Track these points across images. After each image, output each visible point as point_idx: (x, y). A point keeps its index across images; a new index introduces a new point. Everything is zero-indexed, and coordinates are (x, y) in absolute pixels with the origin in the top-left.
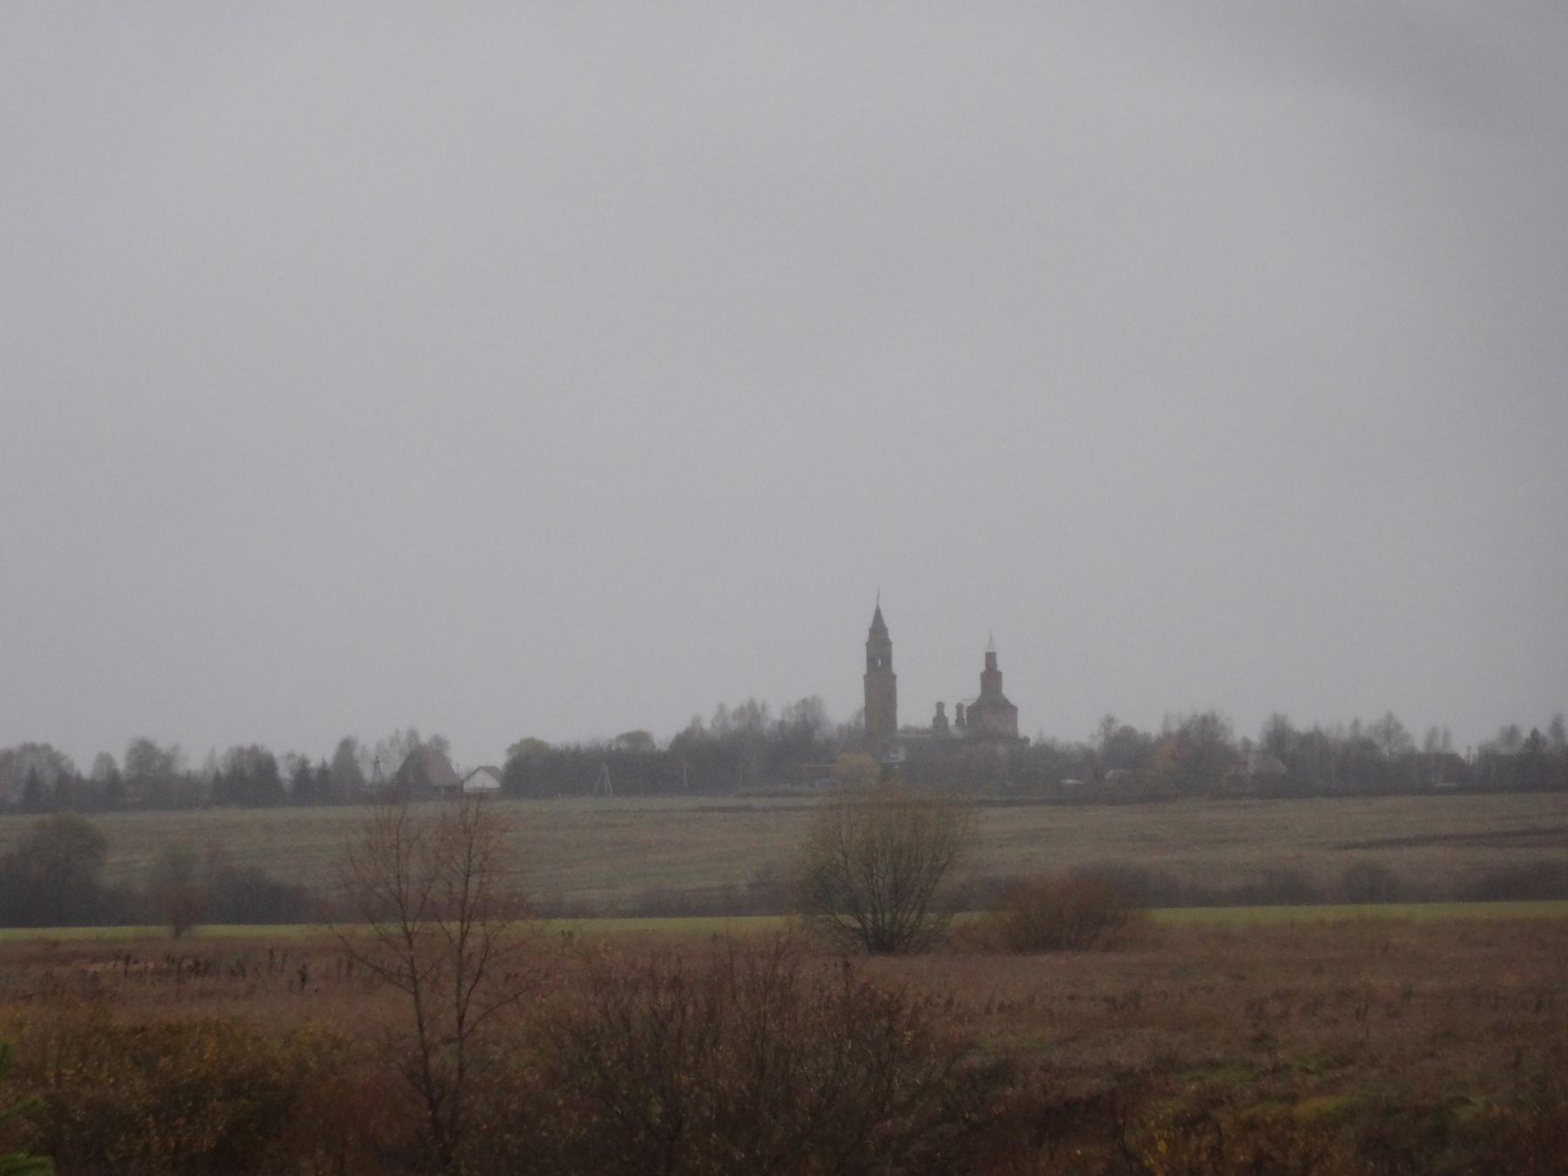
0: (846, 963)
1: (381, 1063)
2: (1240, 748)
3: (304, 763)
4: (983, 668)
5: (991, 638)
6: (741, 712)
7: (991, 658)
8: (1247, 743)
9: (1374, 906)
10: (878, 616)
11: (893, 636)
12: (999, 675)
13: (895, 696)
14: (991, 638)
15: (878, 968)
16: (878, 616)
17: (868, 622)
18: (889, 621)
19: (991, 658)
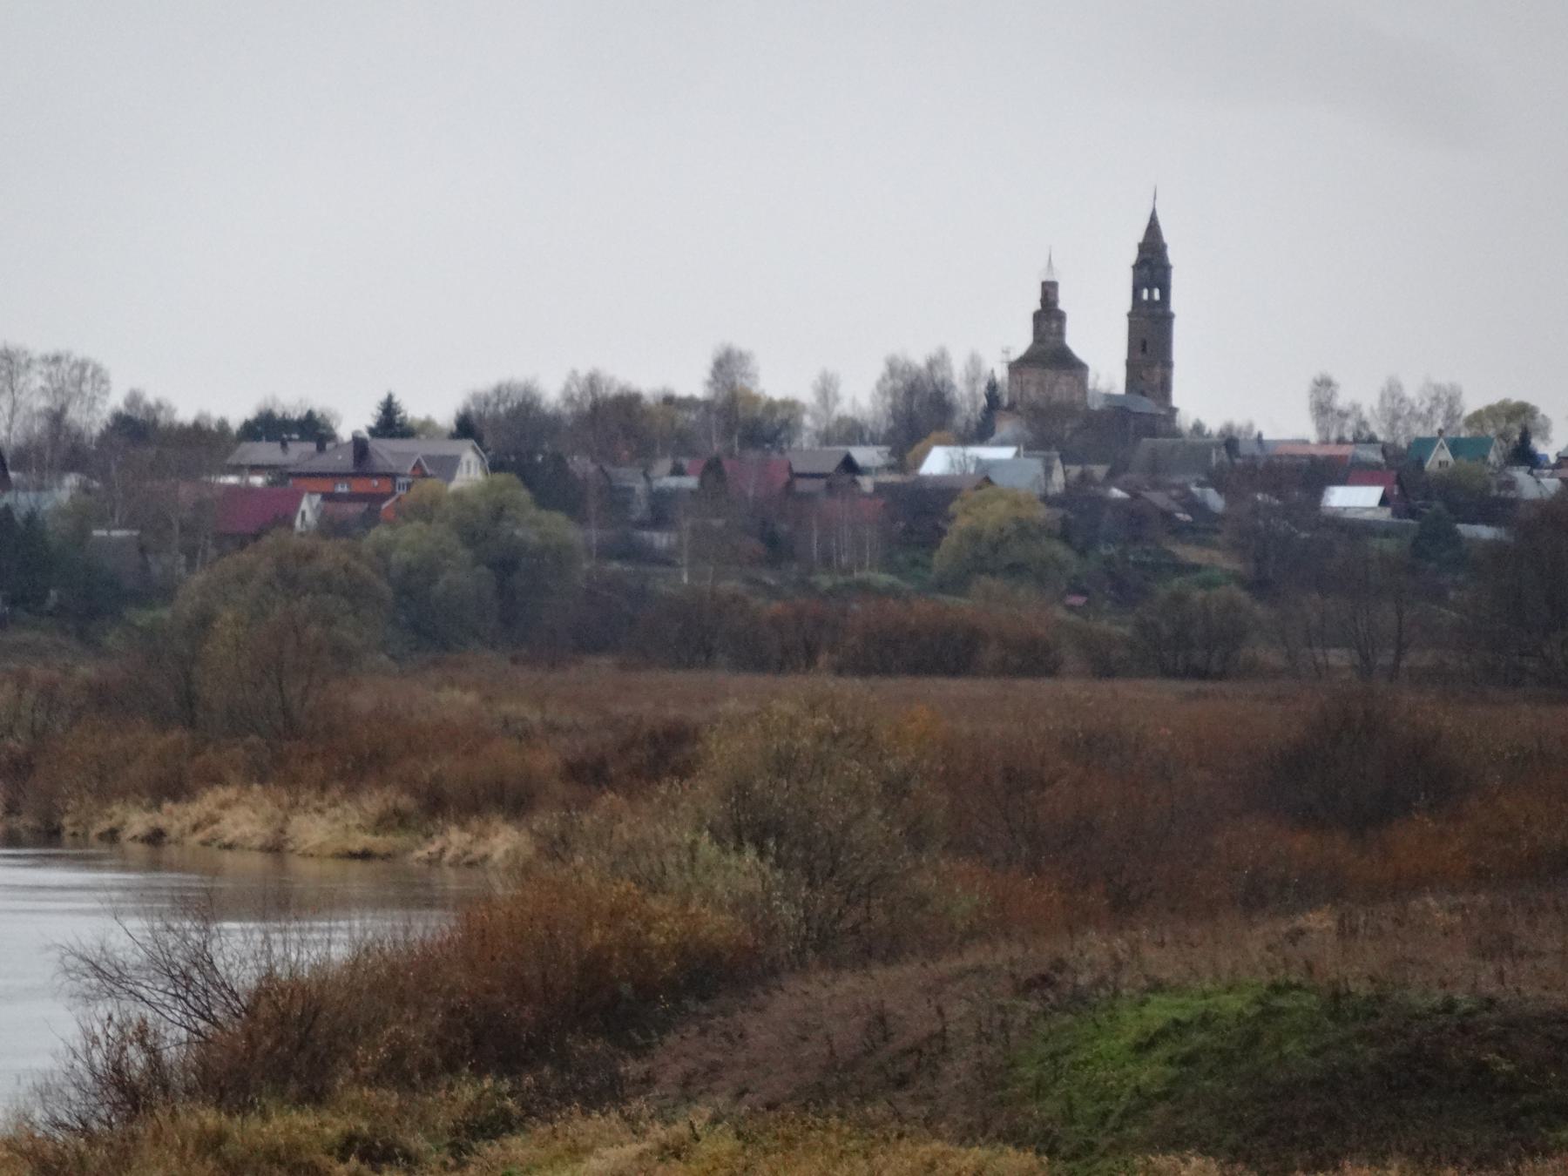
7: (1049, 291)
10: (1153, 229)
11: (1173, 256)
12: (1060, 317)
16: (1153, 229)
19: (1049, 291)
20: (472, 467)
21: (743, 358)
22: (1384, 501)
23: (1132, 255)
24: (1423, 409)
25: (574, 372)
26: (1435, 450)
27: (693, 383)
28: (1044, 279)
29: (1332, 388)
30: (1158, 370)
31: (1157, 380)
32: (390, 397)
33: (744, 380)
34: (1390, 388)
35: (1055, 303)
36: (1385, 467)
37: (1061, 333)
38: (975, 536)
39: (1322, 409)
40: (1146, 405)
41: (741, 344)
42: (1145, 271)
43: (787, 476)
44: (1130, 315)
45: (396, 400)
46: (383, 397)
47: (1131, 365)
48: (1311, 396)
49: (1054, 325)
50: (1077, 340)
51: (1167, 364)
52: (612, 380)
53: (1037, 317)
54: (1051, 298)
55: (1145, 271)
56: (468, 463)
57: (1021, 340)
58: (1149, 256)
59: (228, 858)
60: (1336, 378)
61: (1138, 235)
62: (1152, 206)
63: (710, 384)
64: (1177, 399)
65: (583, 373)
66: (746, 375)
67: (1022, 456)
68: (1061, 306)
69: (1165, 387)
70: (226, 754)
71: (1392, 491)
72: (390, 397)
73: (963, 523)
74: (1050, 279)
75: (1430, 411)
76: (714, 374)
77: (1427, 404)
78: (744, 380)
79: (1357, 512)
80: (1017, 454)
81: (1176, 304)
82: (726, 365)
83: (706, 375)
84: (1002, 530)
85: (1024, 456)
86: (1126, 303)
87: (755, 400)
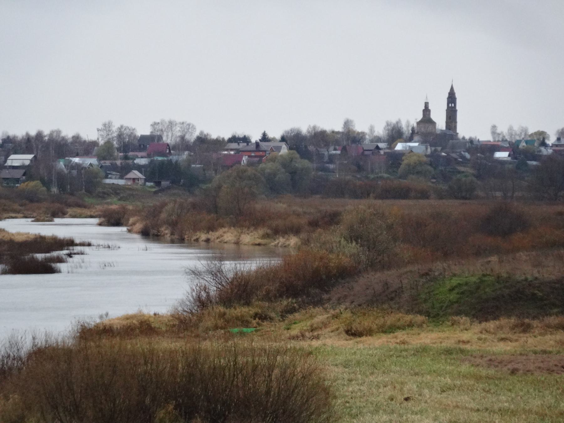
0: (466, 284)
1: (306, 271)
2: (307, 133)
3: (119, 128)
4: (424, 108)
5: (427, 97)
6: (73, 137)
7: (426, 104)
8: (138, 136)
9: (404, 201)
10: (452, 89)
11: (457, 95)
12: (429, 111)
13: (446, 118)
14: (427, 97)
15: (429, 272)
16: (452, 89)
17: (448, 90)
18: (456, 90)
19: (426, 104)
21: (351, 121)
23: (447, 95)
25: (310, 125)
27: (339, 128)
30: (453, 124)
31: (454, 126)
32: (265, 132)
35: (428, 107)
37: (429, 114)
38: (409, 165)
39: (494, 133)
40: (451, 132)
41: (350, 118)
42: (450, 99)
44: (446, 110)
46: (263, 132)
49: (428, 113)
50: (433, 117)
51: (456, 122)
53: (424, 111)
54: (427, 106)
57: (420, 117)
65: (312, 125)
66: (352, 126)
72: (265, 132)
73: (405, 162)
80: (419, 145)
81: (458, 108)
82: (347, 123)
83: (342, 126)
86: (445, 107)
87: (354, 132)
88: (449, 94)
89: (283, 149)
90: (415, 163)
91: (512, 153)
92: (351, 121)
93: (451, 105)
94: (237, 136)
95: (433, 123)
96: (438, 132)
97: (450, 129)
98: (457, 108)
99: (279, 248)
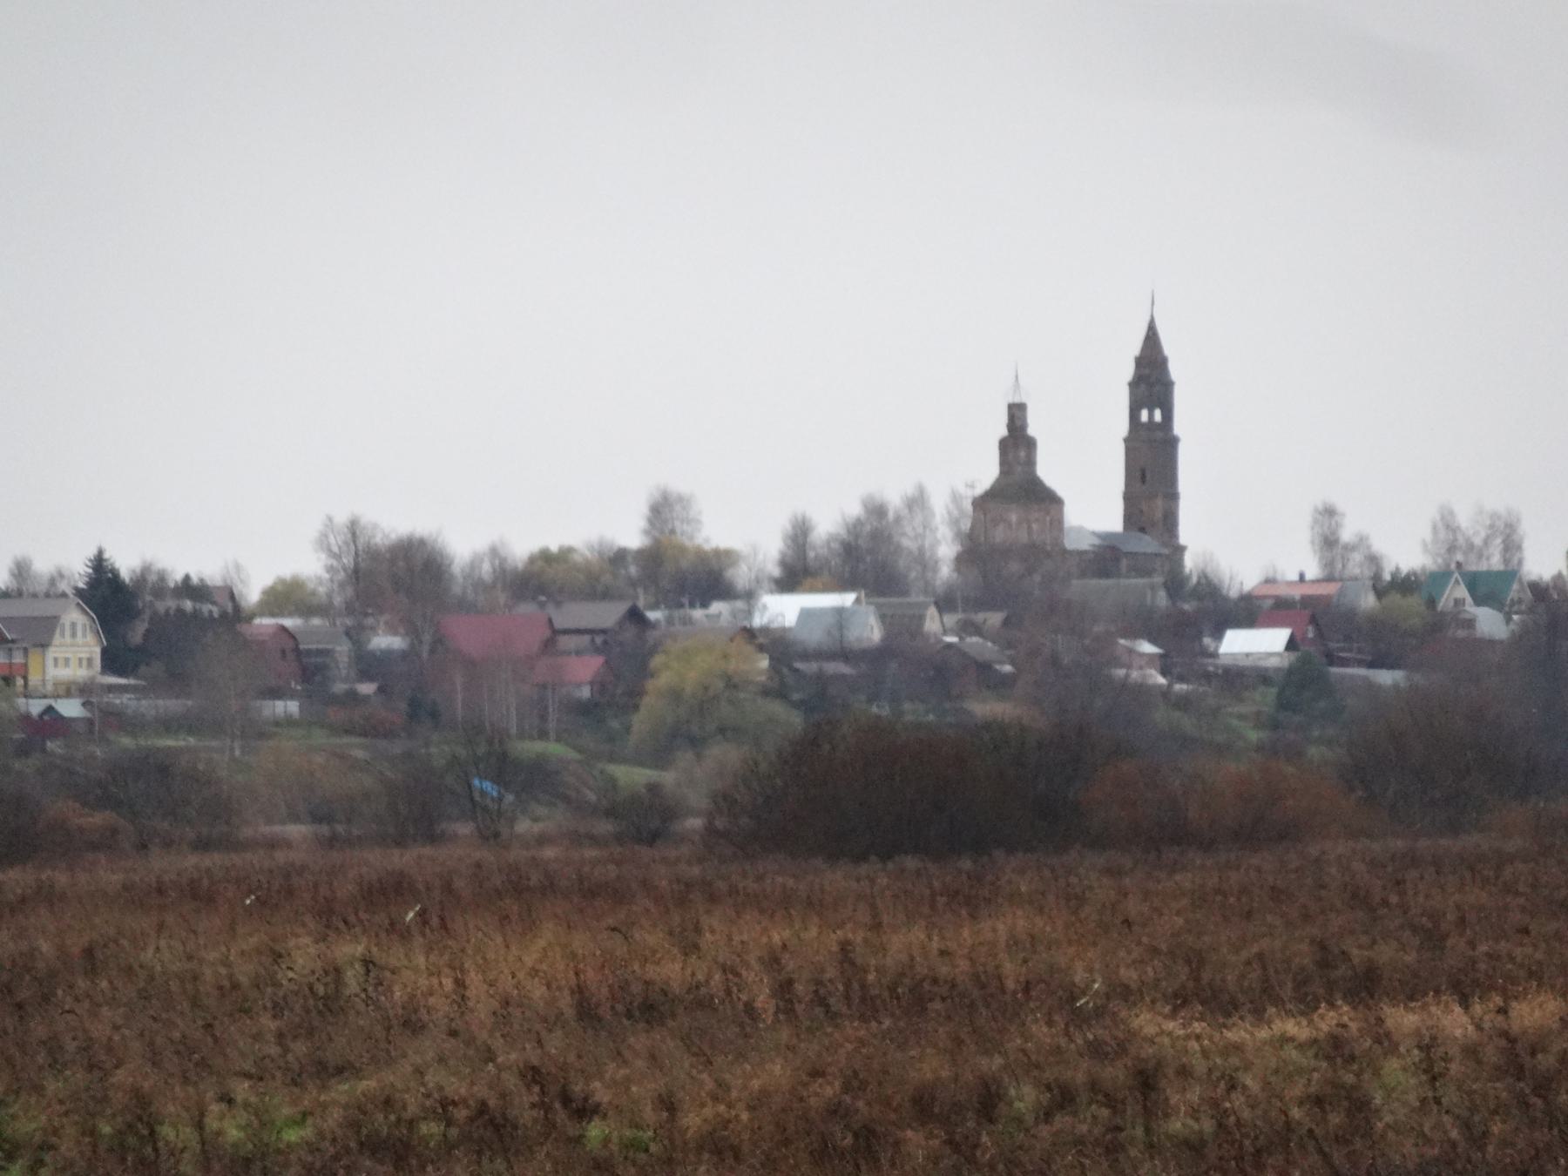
5: (1017, 377)
7: (1016, 414)
10: (1152, 339)
11: (1175, 370)
12: (1030, 444)
14: (1017, 377)
16: (1152, 339)
18: (1168, 347)
19: (1016, 414)
20: (79, 633)
21: (685, 502)
22: (1291, 645)
23: (1128, 371)
24: (1478, 541)
25: (330, 519)
26: (1449, 588)
27: (631, 535)
28: (1011, 401)
29: (1336, 518)
30: (1159, 502)
31: (1159, 515)
32: (100, 552)
33: (685, 527)
34: (1443, 518)
35: (1024, 427)
36: (1299, 606)
37: (1030, 462)
38: (675, 695)
39: (1329, 543)
40: (1147, 544)
41: (678, 485)
42: (1143, 387)
43: (548, 633)
44: (1126, 440)
45: (106, 555)
46: (91, 552)
47: (1130, 498)
48: (1313, 528)
49: (1022, 454)
50: (1049, 470)
51: (1173, 497)
52: (375, 526)
53: (1004, 445)
54: (1018, 423)
55: (1143, 387)
56: (73, 625)
57: (986, 472)
58: (1147, 371)
59: (256, 1142)
60: (1341, 506)
61: (1135, 347)
62: (1149, 314)
63: (646, 532)
64: (1185, 534)
65: (341, 518)
66: (688, 521)
67: (864, 604)
68: (1032, 431)
69: (1169, 523)
70: (1150, 1051)
71: (1306, 633)
72: (100, 552)
73: (664, 680)
74: (1017, 400)
75: (1486, 542)
76: (651, 522)
77: (1483, 534)
78: (685, 527)
79: (1260, 659)
80: (858, 601)
81: (1181, 426)
82: (663, 510)
83: (642, 523)
84: (706, 688)
85: (867, 603)
86: (1122, 427)
87: (682, 550)
88: (1140, 362)
89: (68, 633)
90: (706, 688)
91: (1311, 635)
92: (680, 499)
93: (1151, 415)
94: (195, 580)
95: (1045, 500)
96: (1085, 544)
97: (1142, 530)
98: (1179, 428)
99: (698, 1076)
